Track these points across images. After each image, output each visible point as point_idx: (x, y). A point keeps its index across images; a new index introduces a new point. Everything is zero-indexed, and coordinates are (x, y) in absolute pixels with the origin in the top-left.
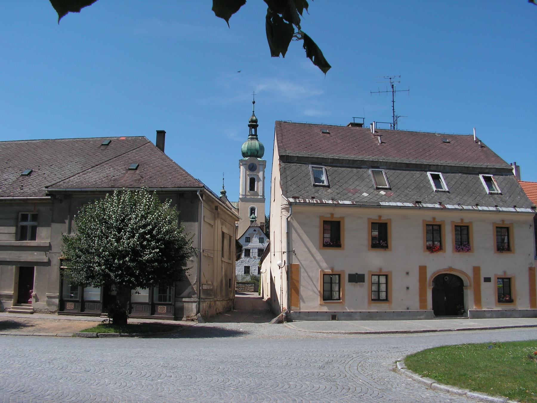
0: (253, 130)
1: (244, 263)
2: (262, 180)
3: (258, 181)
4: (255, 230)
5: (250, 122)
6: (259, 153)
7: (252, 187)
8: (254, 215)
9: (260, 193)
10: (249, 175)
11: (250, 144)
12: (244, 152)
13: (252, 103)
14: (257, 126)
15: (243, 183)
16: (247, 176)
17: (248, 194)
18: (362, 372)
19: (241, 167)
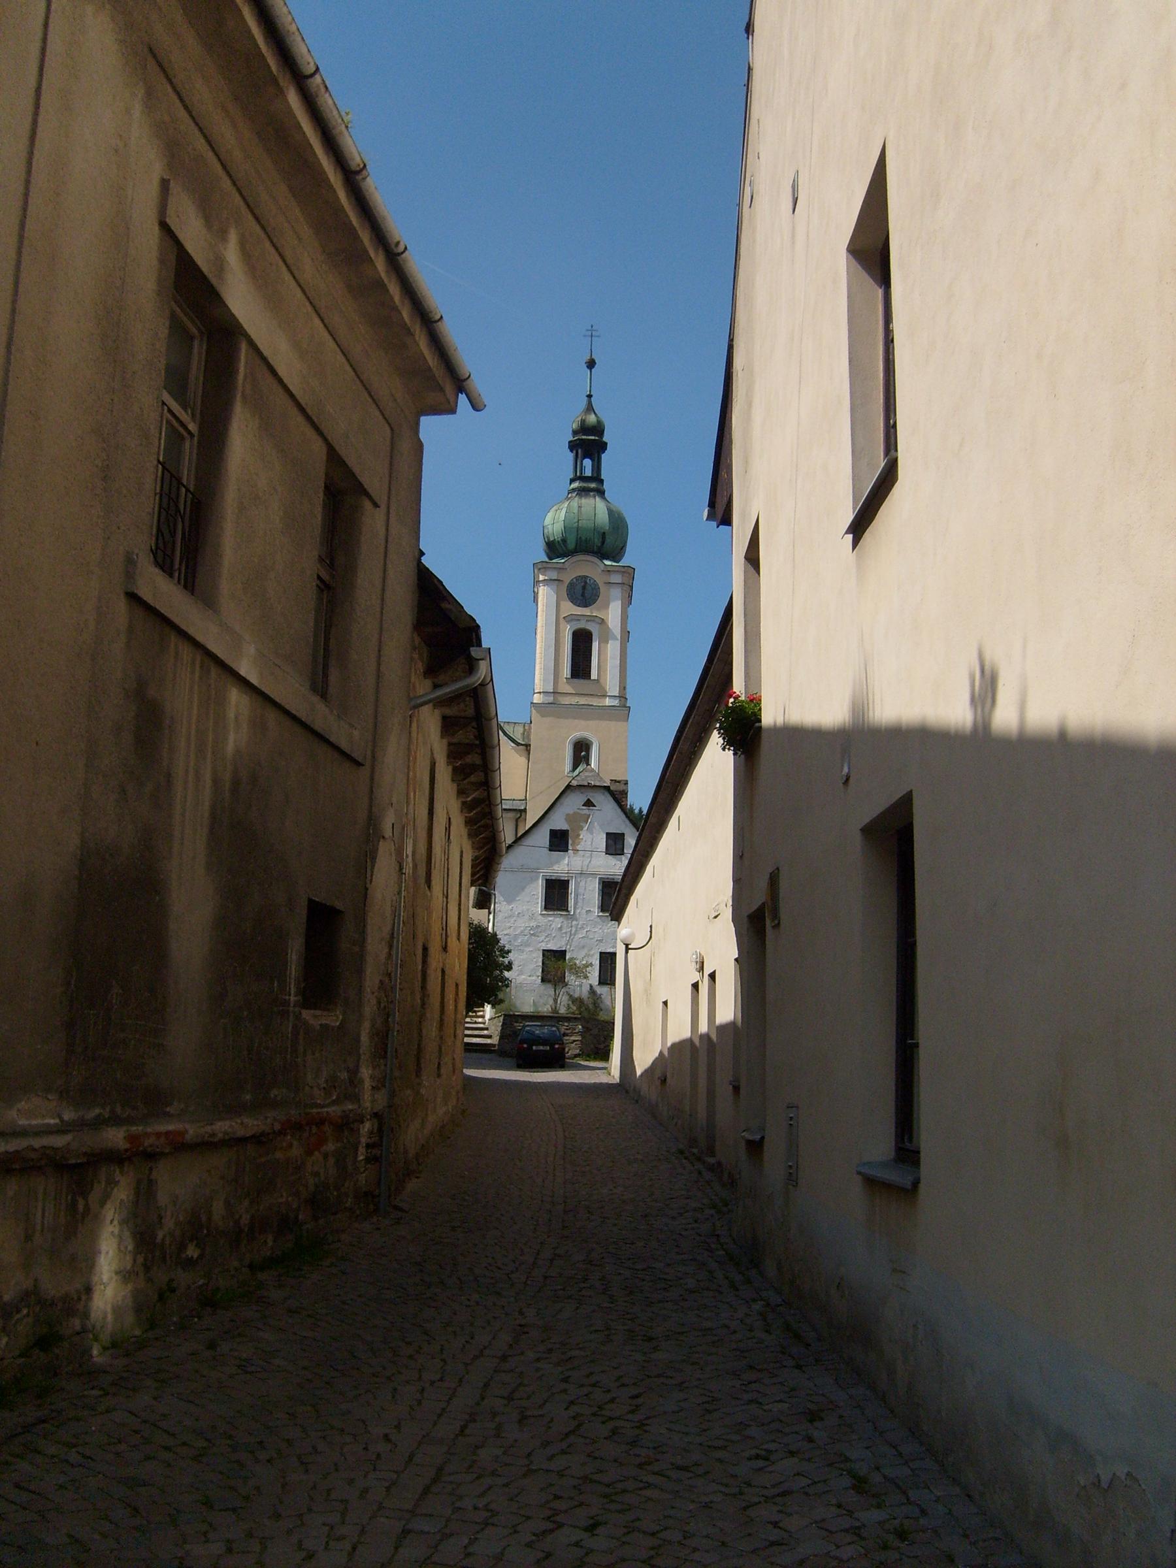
0: (588, 463)
2: (619, 638)
3: (604, 640)
4: (589, 800)
5: (575, 433)
7: (581, 666)
8: (588, 764)
9: (612, 685)
13: (585, 366)
14: (603, 447)
15: (546, 648)
16: (562, 620)
17: (565, 687)
19: (543, 591)
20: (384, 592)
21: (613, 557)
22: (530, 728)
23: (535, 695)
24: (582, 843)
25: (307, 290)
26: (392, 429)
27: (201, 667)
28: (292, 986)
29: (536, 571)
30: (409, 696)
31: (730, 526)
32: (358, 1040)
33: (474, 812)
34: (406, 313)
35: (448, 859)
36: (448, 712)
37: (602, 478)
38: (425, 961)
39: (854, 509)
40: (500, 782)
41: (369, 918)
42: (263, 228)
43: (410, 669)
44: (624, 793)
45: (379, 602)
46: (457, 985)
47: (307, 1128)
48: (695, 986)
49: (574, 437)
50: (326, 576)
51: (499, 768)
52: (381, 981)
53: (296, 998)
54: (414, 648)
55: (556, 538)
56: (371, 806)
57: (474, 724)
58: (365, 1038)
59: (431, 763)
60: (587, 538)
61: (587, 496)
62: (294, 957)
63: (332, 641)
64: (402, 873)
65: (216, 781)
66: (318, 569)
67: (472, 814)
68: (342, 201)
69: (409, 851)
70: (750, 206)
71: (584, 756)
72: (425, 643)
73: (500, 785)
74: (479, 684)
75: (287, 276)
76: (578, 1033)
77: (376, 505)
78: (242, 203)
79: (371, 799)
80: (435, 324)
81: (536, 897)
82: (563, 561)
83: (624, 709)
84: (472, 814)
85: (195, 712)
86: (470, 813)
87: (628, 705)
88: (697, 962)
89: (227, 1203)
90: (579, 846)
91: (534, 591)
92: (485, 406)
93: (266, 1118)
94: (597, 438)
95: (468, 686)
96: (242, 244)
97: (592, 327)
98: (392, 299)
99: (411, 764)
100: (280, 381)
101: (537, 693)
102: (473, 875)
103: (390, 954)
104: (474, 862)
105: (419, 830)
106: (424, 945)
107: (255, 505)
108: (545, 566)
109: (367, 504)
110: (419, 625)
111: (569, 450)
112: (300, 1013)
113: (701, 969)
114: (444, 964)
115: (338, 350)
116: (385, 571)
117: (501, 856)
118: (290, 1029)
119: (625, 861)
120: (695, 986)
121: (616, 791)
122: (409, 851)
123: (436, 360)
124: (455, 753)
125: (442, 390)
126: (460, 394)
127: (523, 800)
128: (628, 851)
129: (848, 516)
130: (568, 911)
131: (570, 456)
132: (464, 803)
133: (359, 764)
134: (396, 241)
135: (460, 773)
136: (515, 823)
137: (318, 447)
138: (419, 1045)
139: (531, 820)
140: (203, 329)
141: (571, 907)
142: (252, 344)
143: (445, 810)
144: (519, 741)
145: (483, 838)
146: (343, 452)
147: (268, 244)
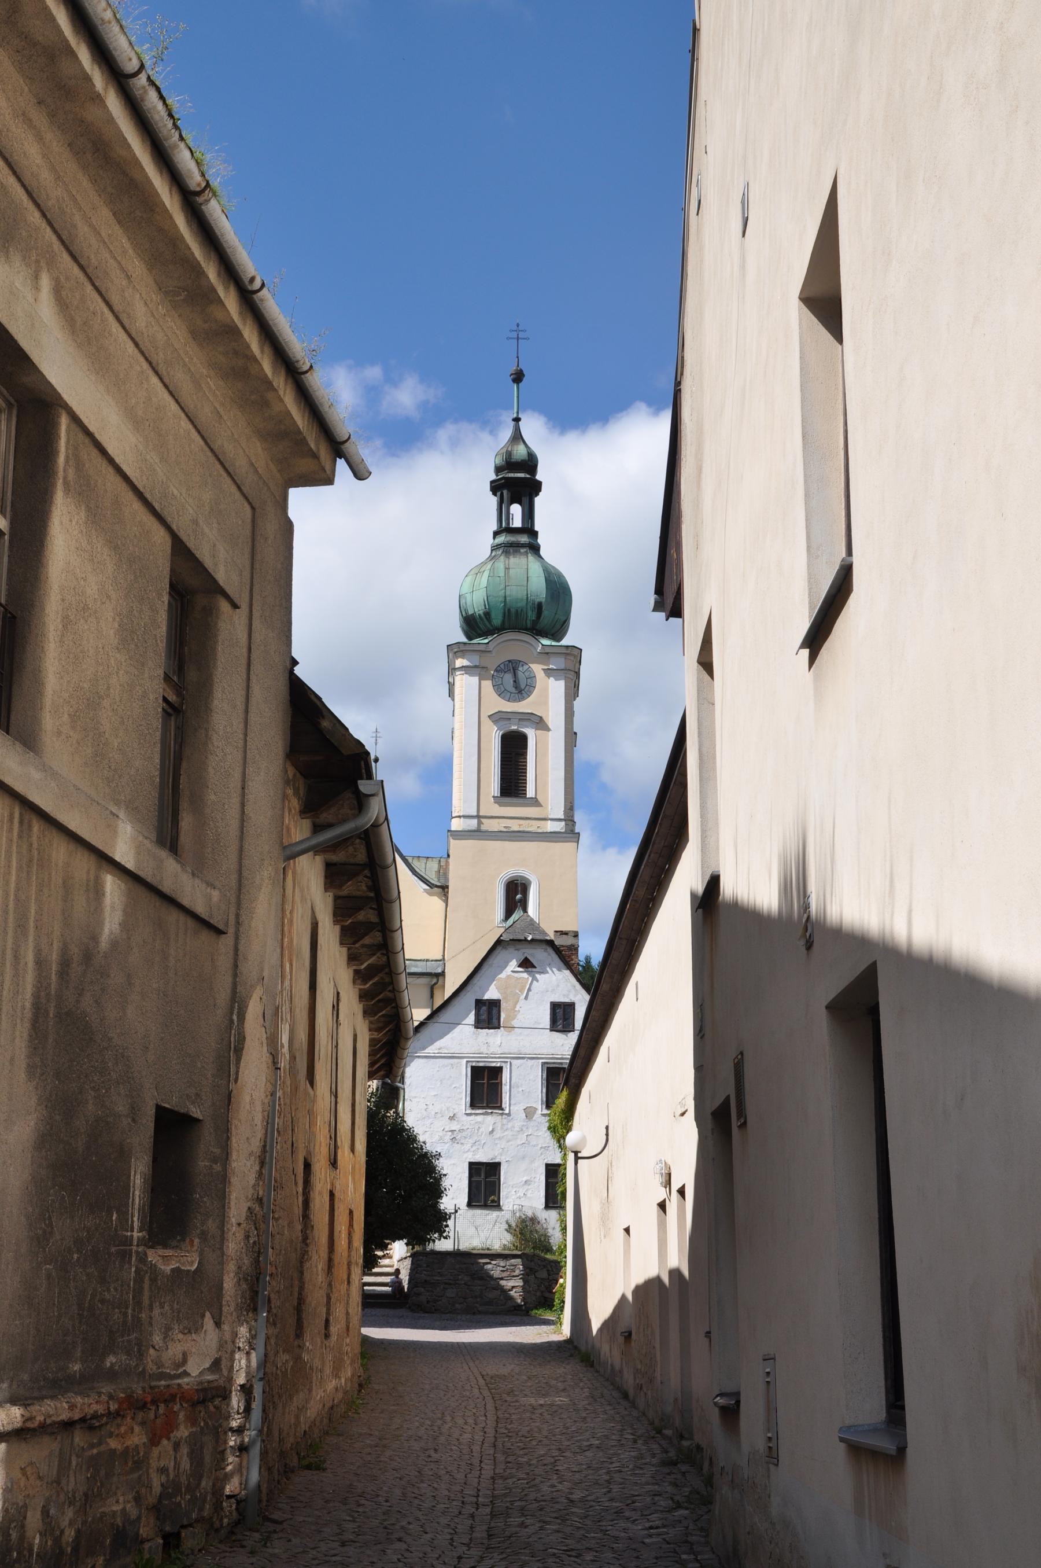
0: (516, 510)
1: (467, 1147)
6: (545, 613)
8: (525, 910)
10: (498, 718)
11: (502, 574)
12: (470, 612)
13: (510, 379)
17: (491, 808)
18: (530, 1530)
20: (247, 715)
21: (553, 635)
22: (447, 863)
23: (453, 820)
24: (519, 1016)
25: (140, 343)
26: (253, 508)
27: (21, 822)
28: (135, 1219)
29: (451, 655)
30: (282, 843)
31: (681, 617)
32: (220, 1287)
33: (371, 983)
34: (267, 365)
35: (337, 1047)
36: (334, 858)
37: (536, 529)
38: (307, 1182)
39: (810, 617)
40: (403, 944)
41: (233, 1127)
42: (82, 268)
43: (283, 808)
44: (574, 949)
45: (242, 726)
46: (351, 1212)
47: (153, 1408)
48: (662, 1206)
49: (497, 476)
50: (172, 698)
51: (401, 926)
52: (249, 1208)
53: (140, 1234)
54: (287, 782)
55: (476, 610)
56: (235, 985)
57: (367, 872)
58: (229, 1284)
59: (312, 924)
60: (517, 611)
61: (516, 552)
62: (138, 1182)
63: (183, 779)
64: (277, 1068)
65: (40, 963)
66: (164, 690)
67: (368, 985)
68: (181, 230)
69: (285, 1039)
70: (698, 214)
71: (520, 901)
72: (301, 774)
73: (403, 948)
74: (371, 825)
75: (115, 327)
76: (518, 1276)
77: (235, 606)
78: (54, 238)
79: (235, 975)
80: (302, 376)
81: (458, 1090)
82: (486, 641)
83: (571, 835)
84: (368, 985)
85: (13, 878)
86: (365, 984)
87: (576, 831)
88: (662, 1174)
89: (45, 1512)
90: (515, 1021)
91: (449, 682)
92: (371, 473)
93: (100, 1394)
94: (528, 476)
95: (357, 829)
96: (57, 291)
97: (518, 325)
98: (248, 347)
99: (286, 929)
100: (111, 461)
101: (456, 817)
102: (371, 1064)
103: (262, 1173)
104: (372, 1048)
105: (298, 1010)
106: (305, 1159)
107: (83, 617)
108: (462, 649)
109: (224, 606)
110: (294, 751)
111: (491, 493)
112: (146, 1254)
113: (668, 1183)
114: (332, 1184)
115: (183, 415)
116: (248, 687)
117: (407, 1039)
118: (133, 1274)
119: (573, 1038)
120: (662, 1206)
121: (563, 946)
122: (285, 1039)
123: (306, 418)
124: (342, 910)
125: (315, 456)
126: (338, 459)
127: (440, 961)
128: (579, 1023)
129: (803, 625)
130: (502, 1109)
131: (494, 500)
132: (357, 972)
133: (219, 932)
134: (250, 276)
135: (350, 935)
136: (429, 990)
137: (160, 537)
138: (300, 1294)
139: (451, 985)
140: (11, 399)
141: (506, 1104)
142: (75, 418)
143: (332, 982)
144: (432, 882)
145: (383, 1016)
146: (191, 544)
147: (89, 288)
